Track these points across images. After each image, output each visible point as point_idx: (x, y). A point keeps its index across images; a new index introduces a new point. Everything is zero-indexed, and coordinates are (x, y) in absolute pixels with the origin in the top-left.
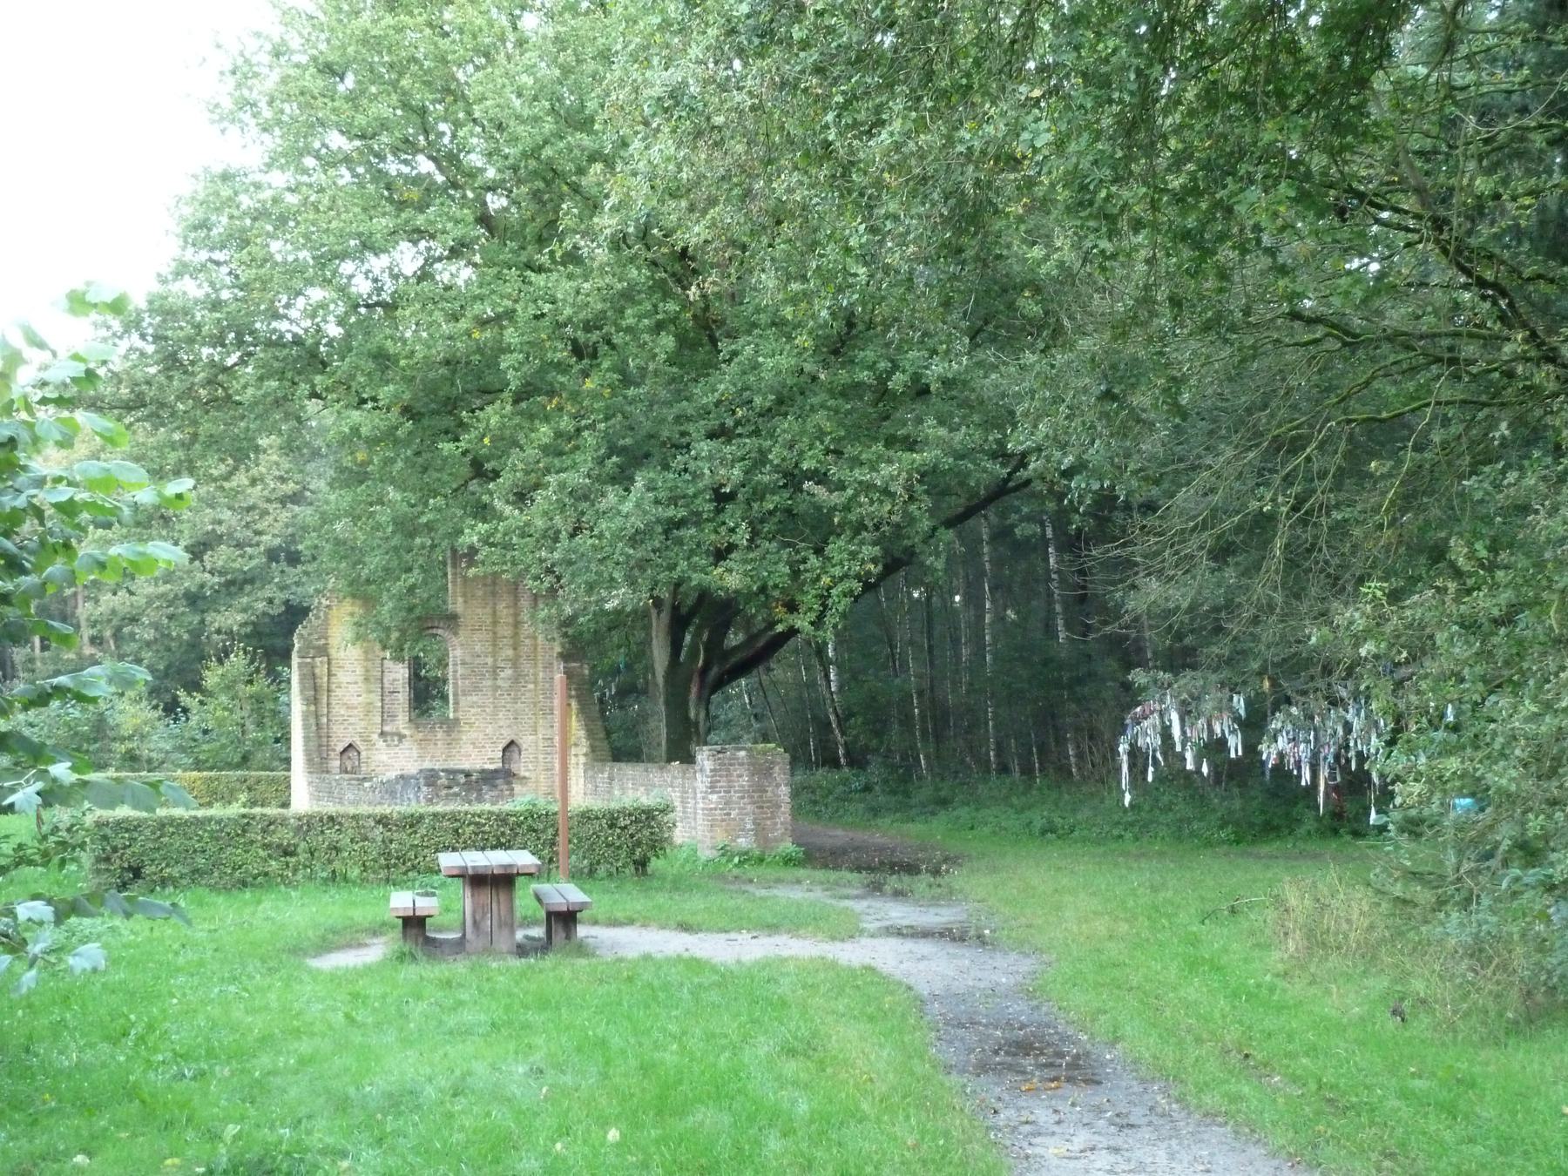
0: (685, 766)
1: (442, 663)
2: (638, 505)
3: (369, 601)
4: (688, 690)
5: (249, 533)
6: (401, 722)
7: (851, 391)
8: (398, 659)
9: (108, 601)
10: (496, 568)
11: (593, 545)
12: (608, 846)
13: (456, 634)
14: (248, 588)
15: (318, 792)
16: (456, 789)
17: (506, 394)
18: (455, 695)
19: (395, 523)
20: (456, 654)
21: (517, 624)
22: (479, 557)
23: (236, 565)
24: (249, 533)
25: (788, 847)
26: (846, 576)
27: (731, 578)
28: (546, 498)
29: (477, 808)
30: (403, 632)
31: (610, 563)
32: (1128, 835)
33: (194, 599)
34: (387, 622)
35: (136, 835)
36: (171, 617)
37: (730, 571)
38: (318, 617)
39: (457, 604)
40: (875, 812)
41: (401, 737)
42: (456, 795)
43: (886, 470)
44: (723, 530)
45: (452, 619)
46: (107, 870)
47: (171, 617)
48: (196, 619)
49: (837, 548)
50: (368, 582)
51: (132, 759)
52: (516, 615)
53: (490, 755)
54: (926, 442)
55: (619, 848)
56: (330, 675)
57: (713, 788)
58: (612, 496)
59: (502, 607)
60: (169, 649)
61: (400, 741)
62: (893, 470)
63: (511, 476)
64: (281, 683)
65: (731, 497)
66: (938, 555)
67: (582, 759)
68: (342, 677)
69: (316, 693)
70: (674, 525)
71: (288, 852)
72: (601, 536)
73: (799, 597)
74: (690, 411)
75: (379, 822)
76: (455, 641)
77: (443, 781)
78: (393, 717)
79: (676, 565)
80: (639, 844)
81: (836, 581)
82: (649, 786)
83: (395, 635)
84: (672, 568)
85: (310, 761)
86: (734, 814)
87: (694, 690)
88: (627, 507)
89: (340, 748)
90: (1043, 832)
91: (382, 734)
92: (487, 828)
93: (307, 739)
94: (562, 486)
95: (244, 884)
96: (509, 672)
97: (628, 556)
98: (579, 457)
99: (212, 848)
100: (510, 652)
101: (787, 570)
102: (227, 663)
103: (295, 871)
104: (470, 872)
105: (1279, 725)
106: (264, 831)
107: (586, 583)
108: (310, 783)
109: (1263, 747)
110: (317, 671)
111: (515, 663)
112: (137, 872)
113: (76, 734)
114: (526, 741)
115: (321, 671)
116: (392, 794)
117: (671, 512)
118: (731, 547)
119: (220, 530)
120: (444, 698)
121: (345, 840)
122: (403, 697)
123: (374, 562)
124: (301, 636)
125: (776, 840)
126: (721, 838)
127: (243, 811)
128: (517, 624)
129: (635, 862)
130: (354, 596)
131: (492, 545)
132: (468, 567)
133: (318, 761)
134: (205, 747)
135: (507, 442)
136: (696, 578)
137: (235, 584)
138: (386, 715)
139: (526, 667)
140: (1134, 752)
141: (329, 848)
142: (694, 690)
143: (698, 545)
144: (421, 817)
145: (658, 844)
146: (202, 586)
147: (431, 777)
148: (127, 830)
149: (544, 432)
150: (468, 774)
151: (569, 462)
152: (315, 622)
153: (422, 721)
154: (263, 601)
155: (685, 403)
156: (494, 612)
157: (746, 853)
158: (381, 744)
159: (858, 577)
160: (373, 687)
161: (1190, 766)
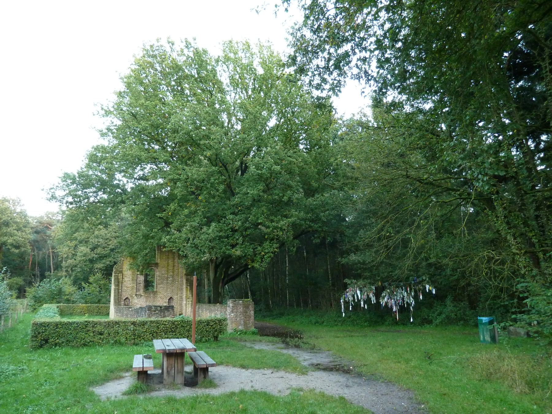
0: (221, 305)
1: (153, 276)
2: (213, 231)
3: (134, 258)
4: (219, 285)
5: (106, 245)
6: (141, 292)
7: (272, 202)
8: (141, 274)
9: (69, 261)
10: (171, 248)
11: (199, 242)
12: (207, 331)
13: (157, 268)
14: (105, 258)
15: (117, 311)
16: (157, 312)
17: (176, 201)
18: (156, 285)
19: (143, 236)
20: (157, 273)
21: (174, 266)
22: (166, 245)
23: (103, 252)
24: (106, 245)
25: (253, 329)
26: (269, 252)
27: (237, 252)
28: (187, 229)
29: (165, 319)
30: (143, 267)
31: (204, 247)
32: (340, 324)
33: (91, 261)
34: (139, 264)
35: (47, 328)
36: (85, 265)
37: (237, 250)
38: (120, 263)
39: (158, 261)
40: (264, 317)
41: (141, 296)
42: (157, 313)
43: (282, 223)
44: (235, 239)
45: (157, 265)
46: (36, 340)
47: (85, 265)
48: (92, 265)
49: (266, 244)
50: (135, 253)
51: (68, 301)
52: (174, 264)
53: (165, 301)
54: (292, 216)
55: (210, 332)
56: (122, 278)
57: (232, 312)
58: (205, 229)
59: (170, 262)
60: (84, 273)
61: (141, 297)
62: (283, 223)
63: (175, 224)
64: (110, 281)
65: (236, 231)
66: (294, 247)
67: (190, 302)
68: (126, 279)
69: (118, 283)
70: (220, 237)
71: (101, 334)
72: (201, 240)
73: (255, 258)
74: (226, 208)
75: (132, 324)
76: (157, 270)
77: (153, 309)
78: (139, 290)
79: (222, 248)
80: (216, 331)
81: (266, 253)
82: (211, 311)
83: (141, 268)
84: (221, 249)
85: (115, 302)
86: (238, 319)
87: (221, 284)
88: (210, 231)
89: (124, 298)
90: (315, 323)
91: (136, 295)
92: (168, 326)
93: (115, 296)
94: (191, 226)
95: (85, 345)
96: (171, 279)
97: (210, 245)
98: (195, 219)
99: (74, 333)
100: (172, 274)
101: (252, 250)
102: (96, 276)
103: (103, 341)
104: (167, 352)
105: (385, 295)
106: (93, 327)
107: (197, 253)
108: (115, 308)
109: (381, 300)
110: (119, 277)
111: (173, 277)
112: (46, 341)
113: (53, 293)
114: (175, 297)
115: (120, 277)
116: (138, 312)
117: (221, 234)
118: (237, 244)
119: (99, 244)
120: (153, 286)
121: (120, 330)
122: (142, 285)
123: (136, 247)
124: (115, 268)
125: (250, 327)
126: (234, 326)
127: (86, 320)
128: (174, 266)
129: (214, 337)
130: (130, 257)
131: (171, 242)
132: (163, 248)
133: (118, 302)
134: (88, 298)
135: (174, 214)
136: (228, 252)
137: (102, 257)
138: (138, 290)
139: (176, 277)
140: (345, 302)
141: (115, 333)
142: (221, 284)
143: (228, 243)
144: (147, 322)
145: (221, 331)
146: (93, 257)
147: (149, 308)
148: (44, 326)
149: (186, 211)
150: (161, 307)
151: (193, 220)
152: (120, 264)
153: (147, 291)
154: (107, 262)
155: (224, 206)
156: (168, 263)
157: (242, 331)
158: (135, 297)
159: (272, 252)
160: (134, 282)
161: (362, 306)
